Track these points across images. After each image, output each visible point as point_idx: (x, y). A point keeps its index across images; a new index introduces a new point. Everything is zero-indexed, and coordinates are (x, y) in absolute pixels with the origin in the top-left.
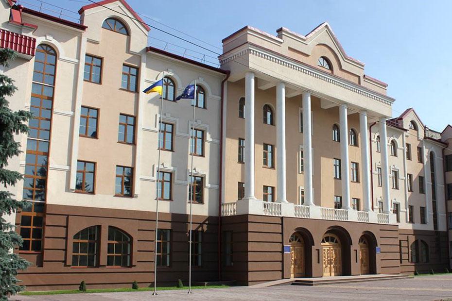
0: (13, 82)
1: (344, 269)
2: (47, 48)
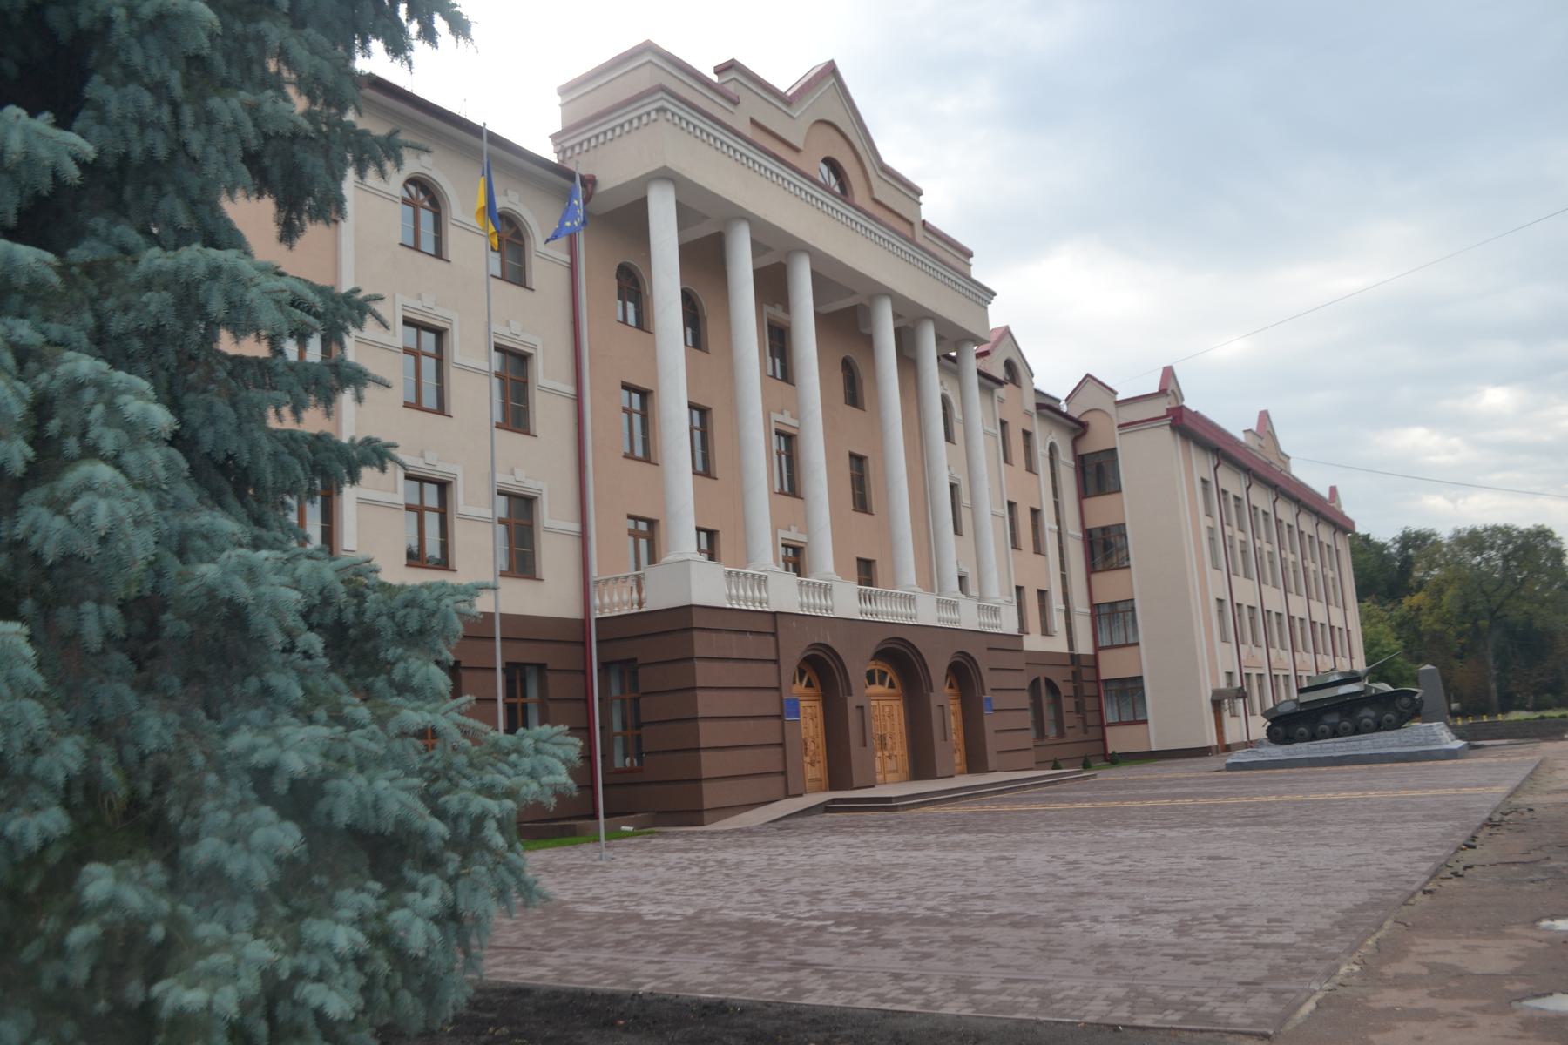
0: (375, 306)
1: (921, 764)
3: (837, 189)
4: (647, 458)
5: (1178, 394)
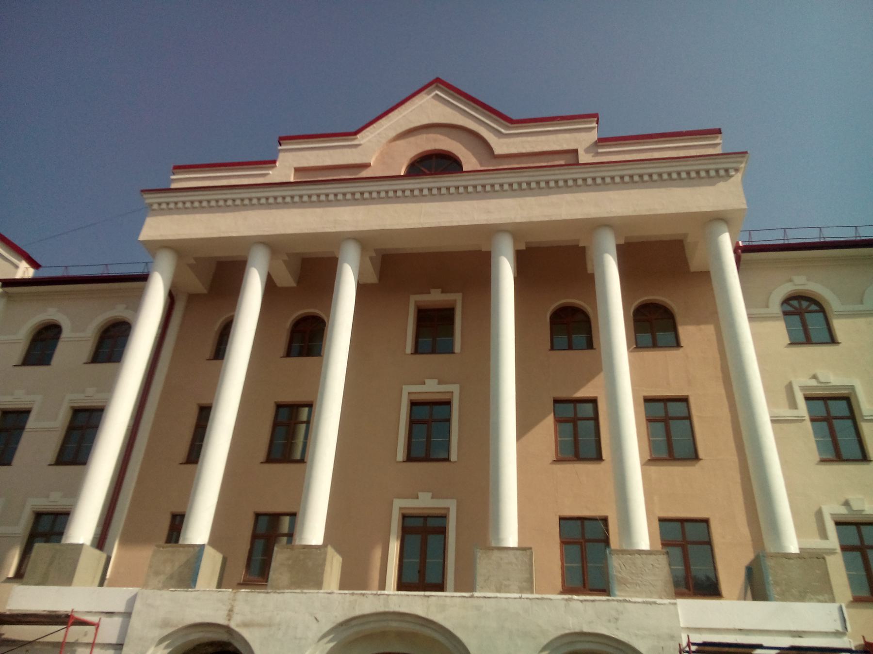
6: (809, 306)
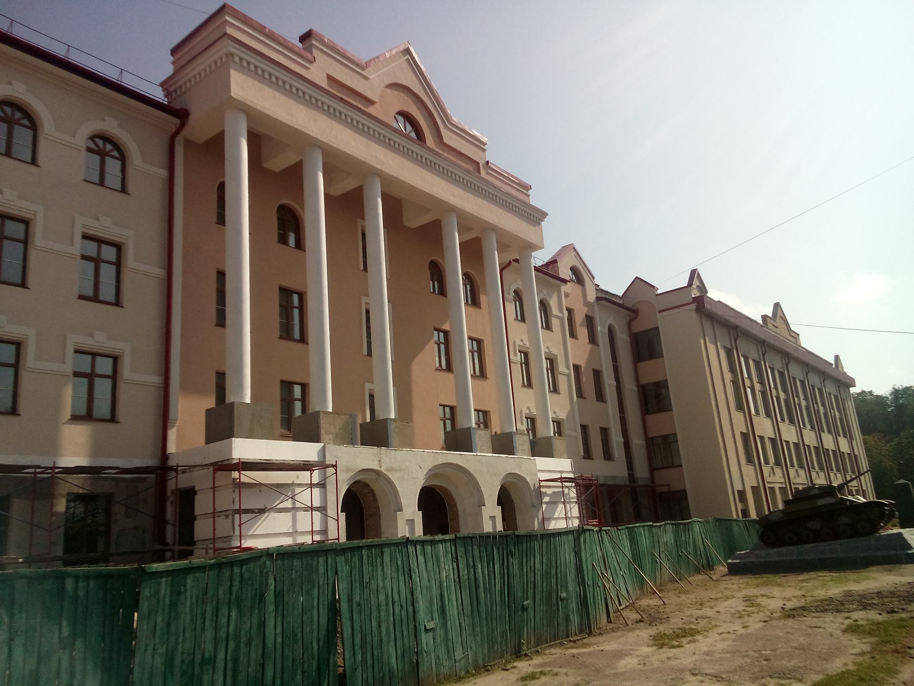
2: (104, 145)
3: (413, 135)
4: (449, 368)
5: (703, 289)
6: (111, 151)
